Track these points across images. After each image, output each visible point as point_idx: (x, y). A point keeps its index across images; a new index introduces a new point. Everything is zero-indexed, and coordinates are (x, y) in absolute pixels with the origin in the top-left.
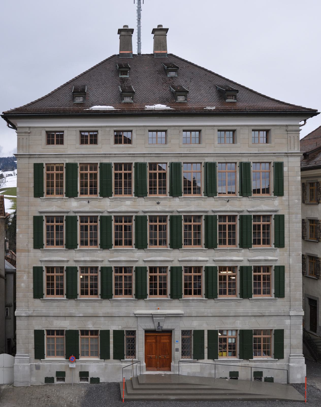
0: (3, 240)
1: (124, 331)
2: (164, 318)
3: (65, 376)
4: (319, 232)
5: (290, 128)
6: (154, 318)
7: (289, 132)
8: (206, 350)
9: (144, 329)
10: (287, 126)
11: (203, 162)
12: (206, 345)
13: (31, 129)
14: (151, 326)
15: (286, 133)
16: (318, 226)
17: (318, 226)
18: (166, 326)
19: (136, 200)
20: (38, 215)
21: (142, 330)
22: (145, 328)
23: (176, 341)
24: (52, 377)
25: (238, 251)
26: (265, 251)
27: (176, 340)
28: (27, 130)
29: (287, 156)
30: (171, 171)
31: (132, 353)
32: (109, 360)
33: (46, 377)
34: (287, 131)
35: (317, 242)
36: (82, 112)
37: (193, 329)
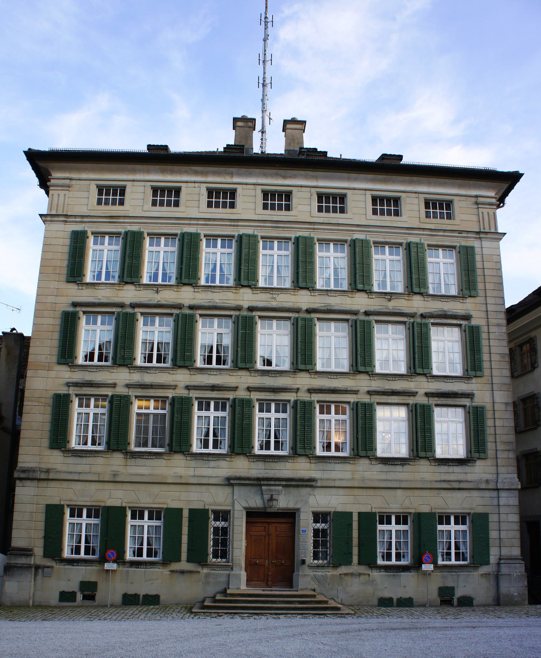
0: (30, 508)
1: (208, 510)
2: (281, 488)
3: (96, 591)
4: (537, 411)
5: (481, 200)
6: (264, 488)
7: (480, 206)
8: (355, 551)
9: (245, 508)
10: (477, 197)
11: (352, 401)
12: (355, 541)
13: (73, 182)
14: (256, 501)
15: (476, 206)
16: (536, 402)
17: (536, 402)
18: (284, 501)
19: (238, 291)
20: (71, 309)
21: (242, 509)
22: (247, 506)
23: (303, 531)
24: (73, 592)
25: (409, 379)
26: (454, 381)
27: (302, 529)
28: (67, 182)
29: (480, 238)
30: (298, 273)
31: (223, 551)
32: (179, 563)
33: (61, 591)
34: (477, 203)
35: (536, 428)
36: (177, 422)
37: (332, 510)
